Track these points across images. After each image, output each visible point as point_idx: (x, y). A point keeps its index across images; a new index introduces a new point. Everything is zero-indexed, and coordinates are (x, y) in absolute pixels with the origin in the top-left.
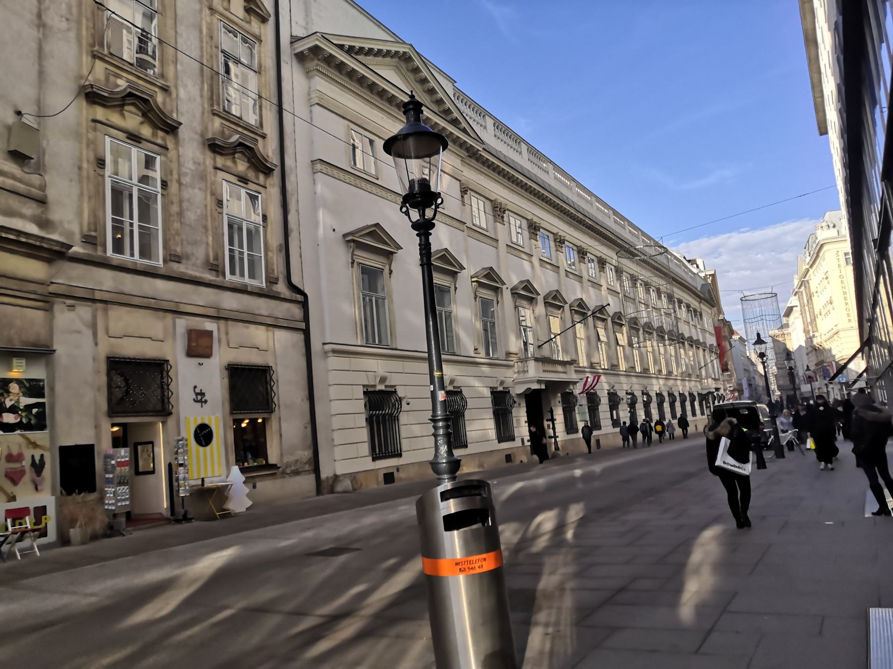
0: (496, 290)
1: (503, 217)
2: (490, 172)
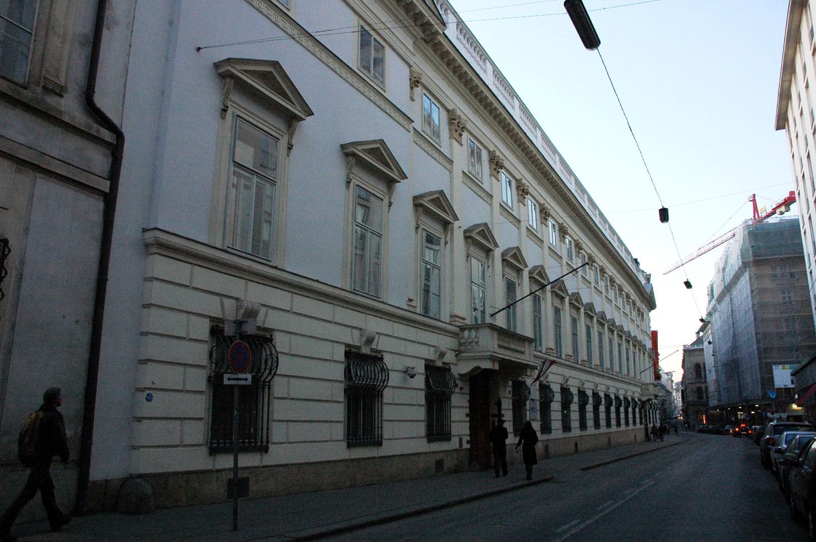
0: (446, 225)
1: (461, 135)
2: (498, 128)
